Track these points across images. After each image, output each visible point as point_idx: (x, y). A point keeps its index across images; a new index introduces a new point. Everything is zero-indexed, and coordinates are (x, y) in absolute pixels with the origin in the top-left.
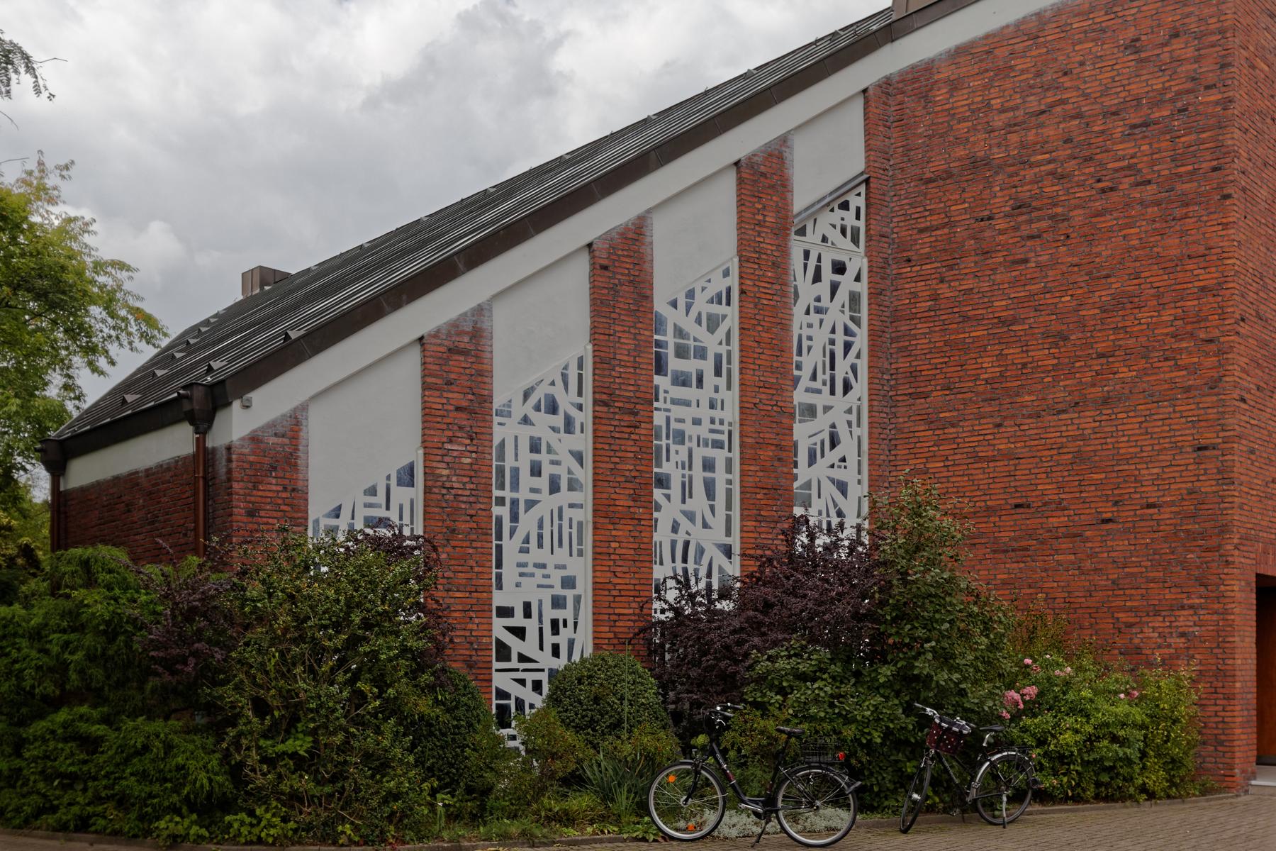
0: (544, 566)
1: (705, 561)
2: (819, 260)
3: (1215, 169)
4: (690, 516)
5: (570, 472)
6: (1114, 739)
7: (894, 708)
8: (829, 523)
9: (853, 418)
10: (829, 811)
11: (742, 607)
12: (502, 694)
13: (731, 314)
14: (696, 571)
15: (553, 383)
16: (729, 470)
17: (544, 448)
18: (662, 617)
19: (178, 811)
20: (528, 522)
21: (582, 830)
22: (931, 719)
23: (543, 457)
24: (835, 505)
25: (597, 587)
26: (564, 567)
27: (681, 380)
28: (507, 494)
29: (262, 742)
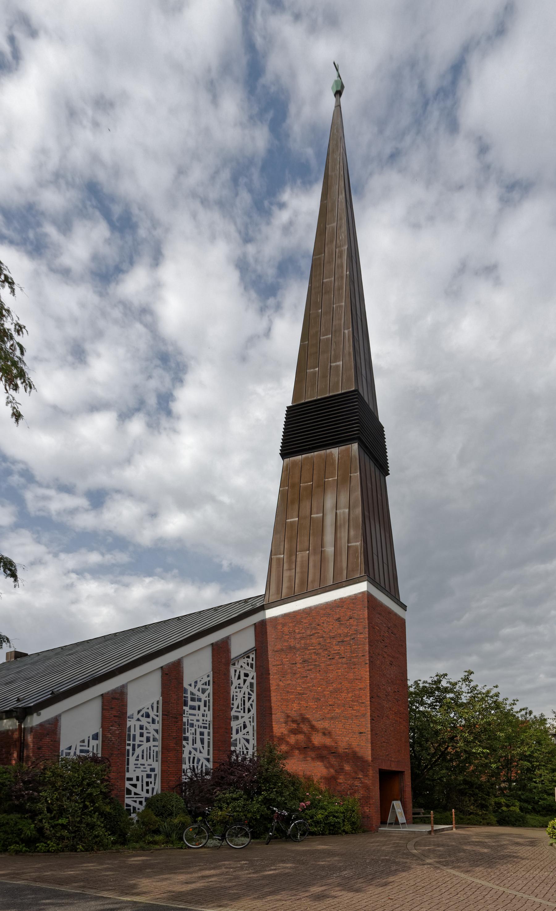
0: (144, 765)
1: (200, 763)
2: (240, 673)
3: (363, 656)
4: (195, 749)
5: (153, 736)
6: (334, 816)
7: (264, 808)
8: (243, 752)
9: (251, 720)
10: (243, 839)
11: (213, 778)
12: (128, 805)
13: (210, 689)
14: (197, 767)
15: (148, 709)
16: (209, 735)
17: (144, 728)
18: (186, 781)
19: (18, 843)
20: (138, 751)
21: (161, 846)
22: (275, 811)
23: (144, 731)
24: (245, 746)
25: (163, 771)
26: (151, 765)
27: (192, 708)
28: (131, 742)
29: (50, 821)
